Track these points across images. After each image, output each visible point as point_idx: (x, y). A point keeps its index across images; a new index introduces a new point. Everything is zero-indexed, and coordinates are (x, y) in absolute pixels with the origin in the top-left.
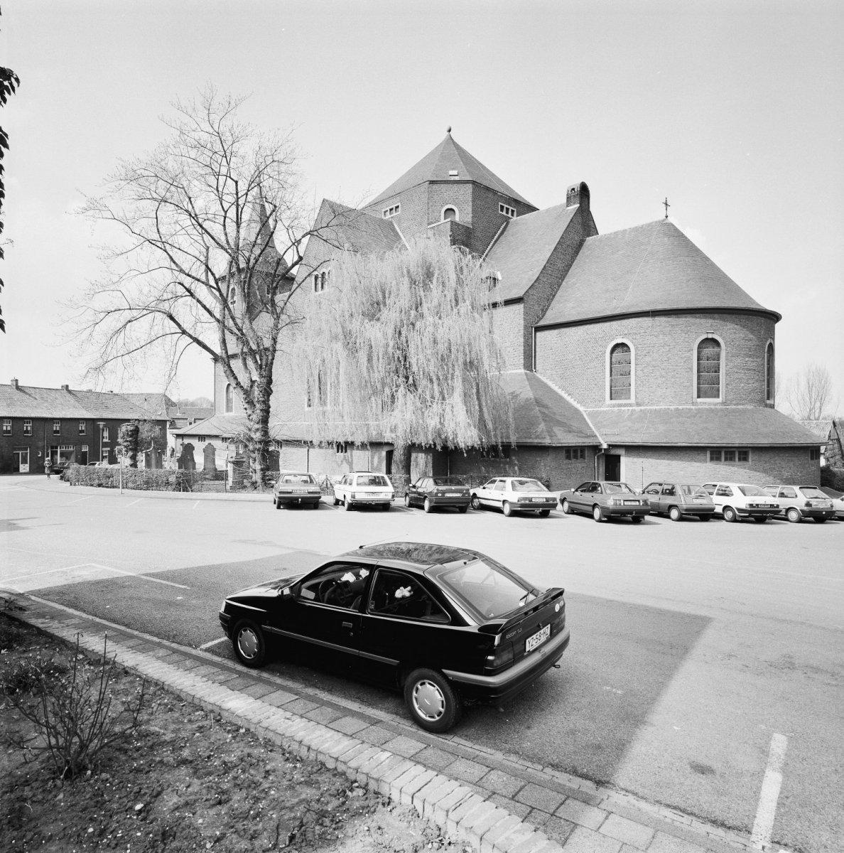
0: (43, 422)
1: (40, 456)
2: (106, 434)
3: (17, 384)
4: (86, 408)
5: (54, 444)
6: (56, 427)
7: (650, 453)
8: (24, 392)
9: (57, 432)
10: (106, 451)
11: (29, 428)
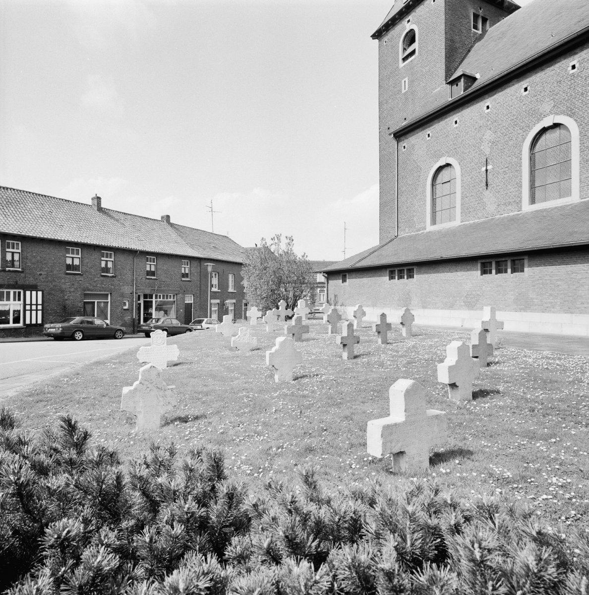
0: (131, 258)
1: (125, 308)
2: (215, 281)
3: (99, 203)
4: (192, 246)
5: (148, 292)
6: (74, 258)
7: (441, 268)
8: (110, 216)
9: (185, 275)
10: (215, 304)
11: (110, 265)
